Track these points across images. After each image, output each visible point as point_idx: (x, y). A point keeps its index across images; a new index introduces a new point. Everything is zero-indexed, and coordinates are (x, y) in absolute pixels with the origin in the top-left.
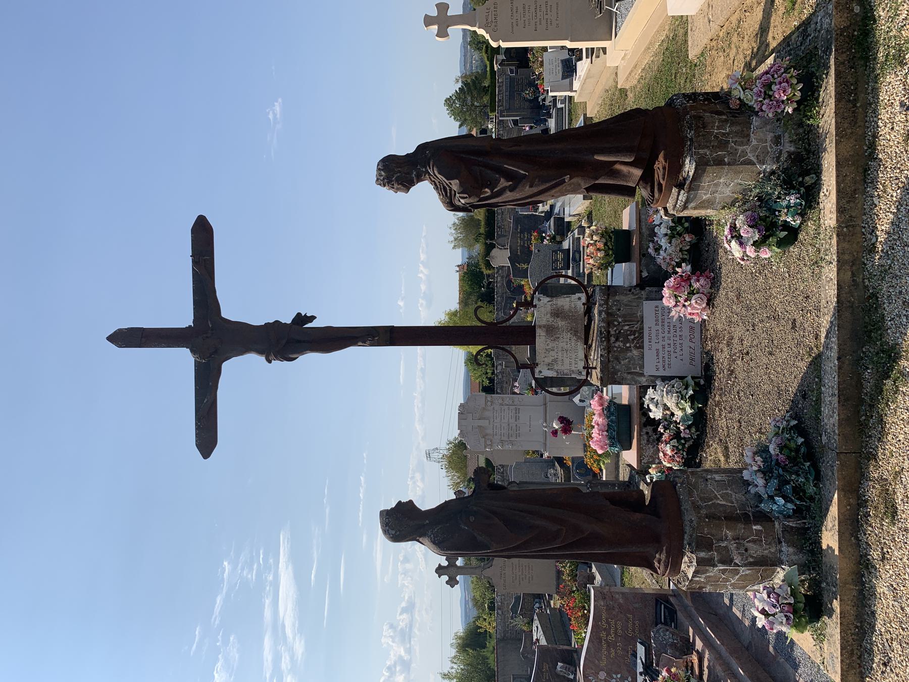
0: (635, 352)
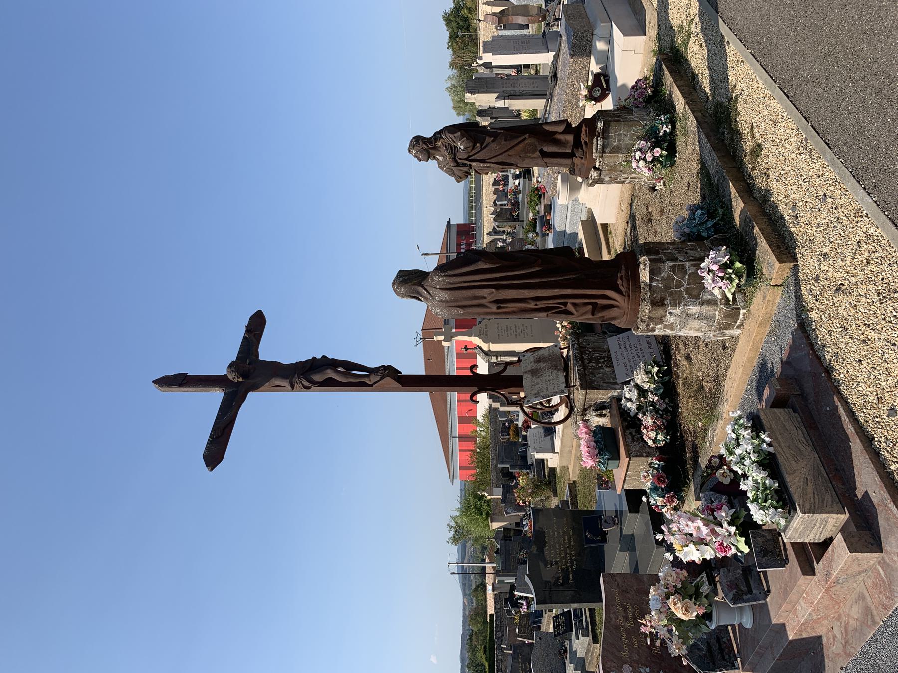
0: (607, 370)
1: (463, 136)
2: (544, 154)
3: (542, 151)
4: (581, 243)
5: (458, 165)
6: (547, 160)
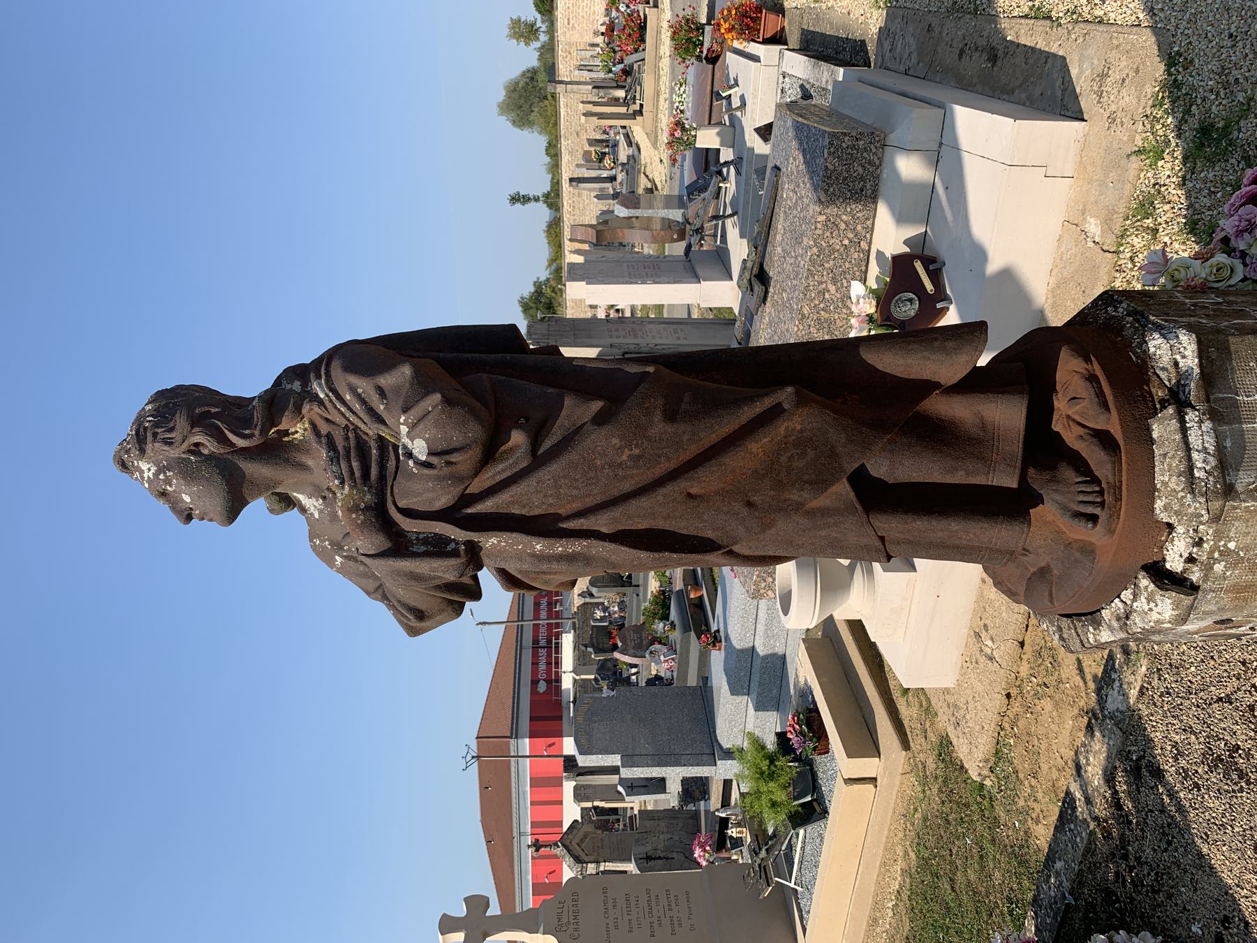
1: (423, 385)
2: (876, 497)
3: (861, 482)
4: (806, 693)
5: (399, 546)
6: (892, 526)
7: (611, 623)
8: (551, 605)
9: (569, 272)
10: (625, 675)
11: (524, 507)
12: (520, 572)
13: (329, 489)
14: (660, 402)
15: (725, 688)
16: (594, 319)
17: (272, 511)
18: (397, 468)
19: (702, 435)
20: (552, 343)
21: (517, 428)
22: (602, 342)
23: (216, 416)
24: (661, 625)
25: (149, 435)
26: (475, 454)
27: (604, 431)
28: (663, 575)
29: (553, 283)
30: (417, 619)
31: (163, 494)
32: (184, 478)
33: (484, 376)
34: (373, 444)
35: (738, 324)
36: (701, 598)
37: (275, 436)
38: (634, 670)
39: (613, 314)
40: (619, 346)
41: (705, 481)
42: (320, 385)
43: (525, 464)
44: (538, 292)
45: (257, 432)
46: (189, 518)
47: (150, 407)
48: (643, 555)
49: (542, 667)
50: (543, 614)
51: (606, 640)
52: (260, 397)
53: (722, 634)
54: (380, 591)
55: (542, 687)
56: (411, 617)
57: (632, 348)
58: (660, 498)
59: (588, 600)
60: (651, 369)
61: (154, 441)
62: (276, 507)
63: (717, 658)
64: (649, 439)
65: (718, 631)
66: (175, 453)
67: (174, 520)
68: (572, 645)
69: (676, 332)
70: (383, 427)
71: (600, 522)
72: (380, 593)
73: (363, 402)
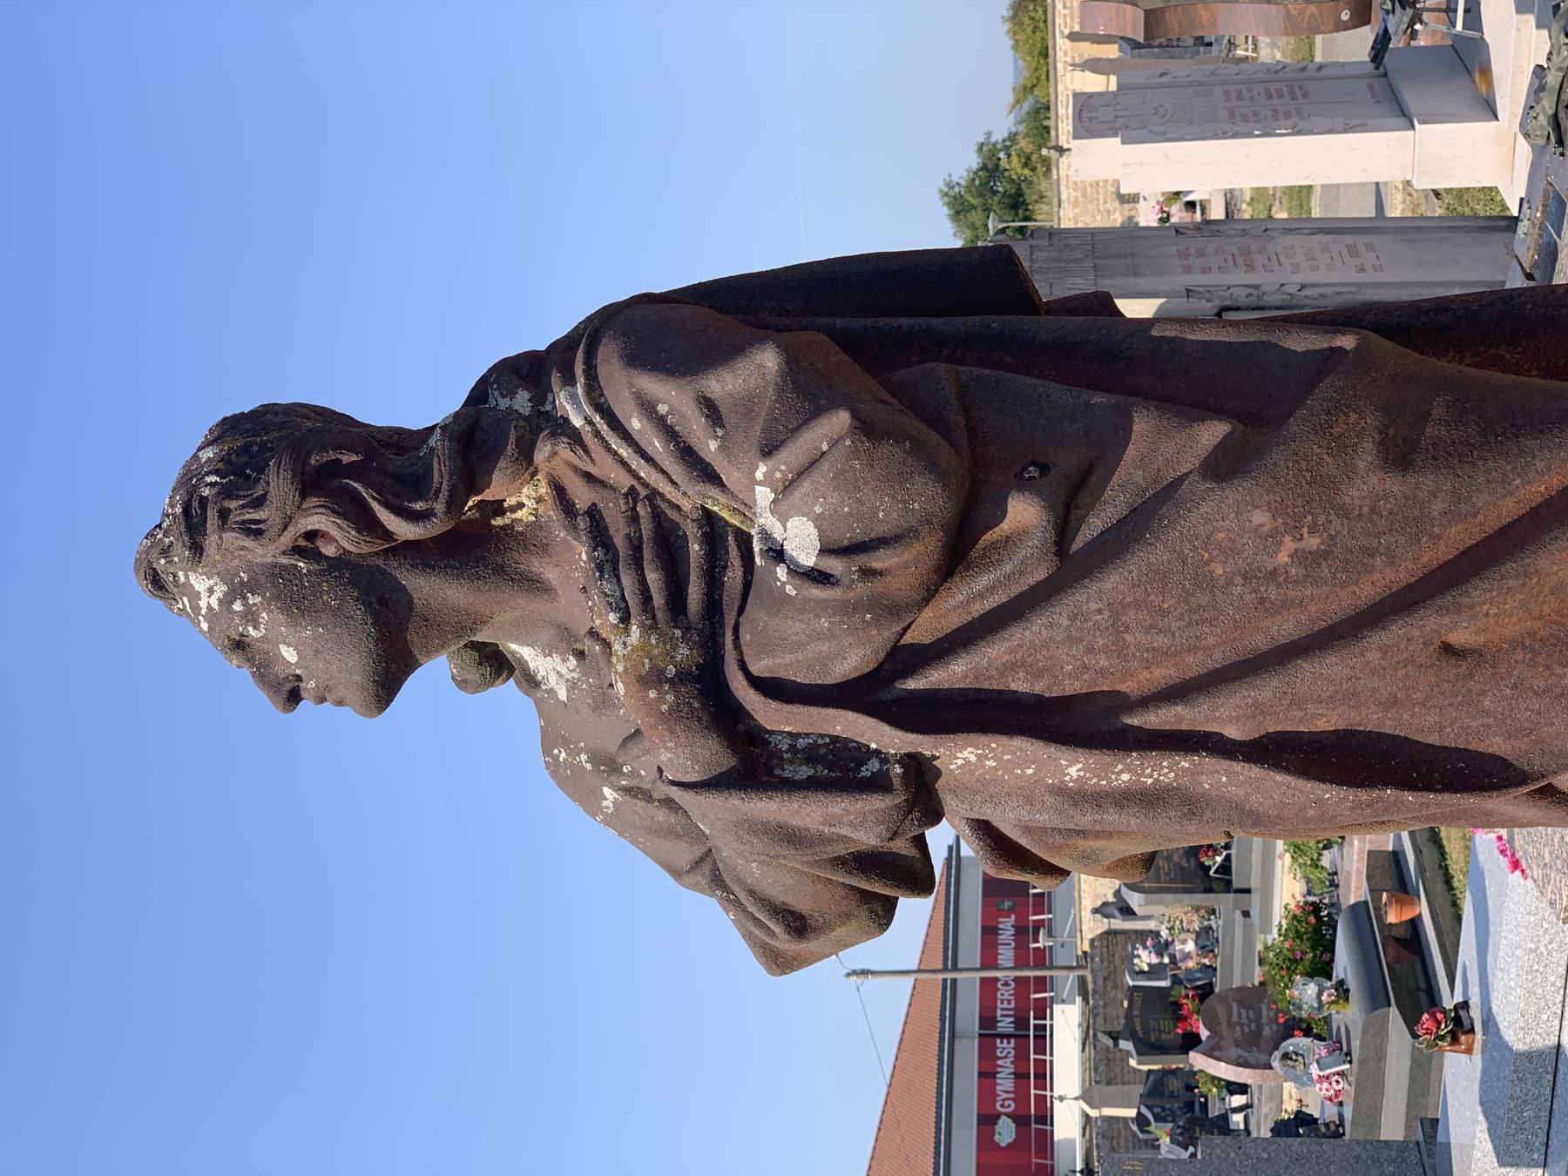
1: (806, 394)
5: (752, 764)
7: (1176, 981)
8: (1024, 933)
9: (1079, 116)
10: (1214, 1111)
11: (1039, 675)
12: (1027, 830)
13: (593, 634)
14: (1372, 420)
15: (1484, 1146)
16: (1131, 231)
17: (462, 684)
18: (747, 586)
19: (1480, 500)
20: (1104, 285)
21: (1020, 489)
22: (1165, 283)
23: (352, 470)
24: (1312, 989)
25: (212, 515)
26: (924, 551)
27: (1234, 493)
28: (1316, 865)
29: (1025, 145)
30: (789, 933)
31: (239, 645)
32: (285, 610)
33: (942, 369)
34: (692, 531)
35: (1523, 227)
36: (1415, 924)
37: (474, 514)
38: (1238, 1100)
39: (1178, 215)
40: (1209, 292)
41: (1488, 614)
42: (573, 398)
43: (1041, 575)
44: (990, 170)
45: (439, 507)
46: (294, 697)
47: (209, 453)
48: (1330, 794)
49: (1005, 1083)
50: (1006, 955)
51: (1165, 1024)
52: (444, 427)
53: (1476, 1013)
54: (706, 868)
55: (1005, 1132)
56: (777, 929)
57: (1240, 295)
58: (1374, 656)
59: (1119, 924)
60: (1347, 342)
61: (222, 528)
62: (473, 675)
63: (1461, 1074)
64: (1344, 513)
65: (1465, 1005)
66: (266, 553)
67: (262, 702)
68: (1077, 1034)
69: (1353, 251)
70: (714, 492)
71: (1224, 712)
72: (709, 872)
73: (670, 433)
